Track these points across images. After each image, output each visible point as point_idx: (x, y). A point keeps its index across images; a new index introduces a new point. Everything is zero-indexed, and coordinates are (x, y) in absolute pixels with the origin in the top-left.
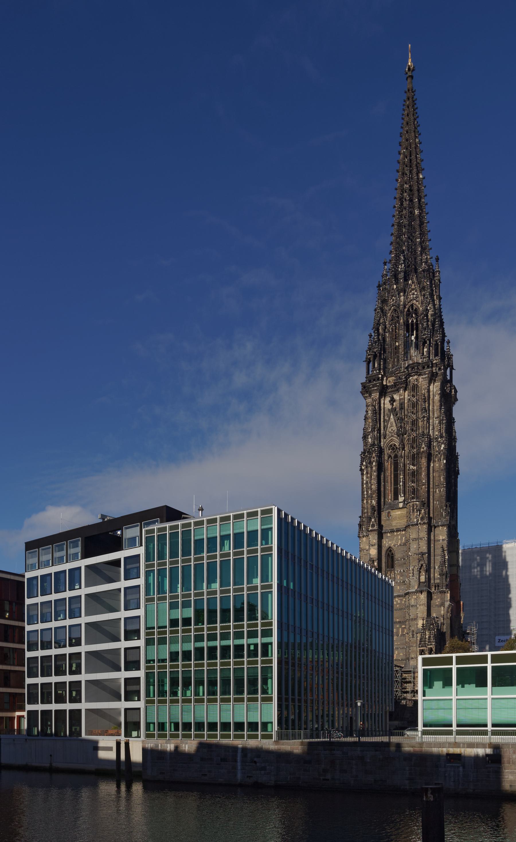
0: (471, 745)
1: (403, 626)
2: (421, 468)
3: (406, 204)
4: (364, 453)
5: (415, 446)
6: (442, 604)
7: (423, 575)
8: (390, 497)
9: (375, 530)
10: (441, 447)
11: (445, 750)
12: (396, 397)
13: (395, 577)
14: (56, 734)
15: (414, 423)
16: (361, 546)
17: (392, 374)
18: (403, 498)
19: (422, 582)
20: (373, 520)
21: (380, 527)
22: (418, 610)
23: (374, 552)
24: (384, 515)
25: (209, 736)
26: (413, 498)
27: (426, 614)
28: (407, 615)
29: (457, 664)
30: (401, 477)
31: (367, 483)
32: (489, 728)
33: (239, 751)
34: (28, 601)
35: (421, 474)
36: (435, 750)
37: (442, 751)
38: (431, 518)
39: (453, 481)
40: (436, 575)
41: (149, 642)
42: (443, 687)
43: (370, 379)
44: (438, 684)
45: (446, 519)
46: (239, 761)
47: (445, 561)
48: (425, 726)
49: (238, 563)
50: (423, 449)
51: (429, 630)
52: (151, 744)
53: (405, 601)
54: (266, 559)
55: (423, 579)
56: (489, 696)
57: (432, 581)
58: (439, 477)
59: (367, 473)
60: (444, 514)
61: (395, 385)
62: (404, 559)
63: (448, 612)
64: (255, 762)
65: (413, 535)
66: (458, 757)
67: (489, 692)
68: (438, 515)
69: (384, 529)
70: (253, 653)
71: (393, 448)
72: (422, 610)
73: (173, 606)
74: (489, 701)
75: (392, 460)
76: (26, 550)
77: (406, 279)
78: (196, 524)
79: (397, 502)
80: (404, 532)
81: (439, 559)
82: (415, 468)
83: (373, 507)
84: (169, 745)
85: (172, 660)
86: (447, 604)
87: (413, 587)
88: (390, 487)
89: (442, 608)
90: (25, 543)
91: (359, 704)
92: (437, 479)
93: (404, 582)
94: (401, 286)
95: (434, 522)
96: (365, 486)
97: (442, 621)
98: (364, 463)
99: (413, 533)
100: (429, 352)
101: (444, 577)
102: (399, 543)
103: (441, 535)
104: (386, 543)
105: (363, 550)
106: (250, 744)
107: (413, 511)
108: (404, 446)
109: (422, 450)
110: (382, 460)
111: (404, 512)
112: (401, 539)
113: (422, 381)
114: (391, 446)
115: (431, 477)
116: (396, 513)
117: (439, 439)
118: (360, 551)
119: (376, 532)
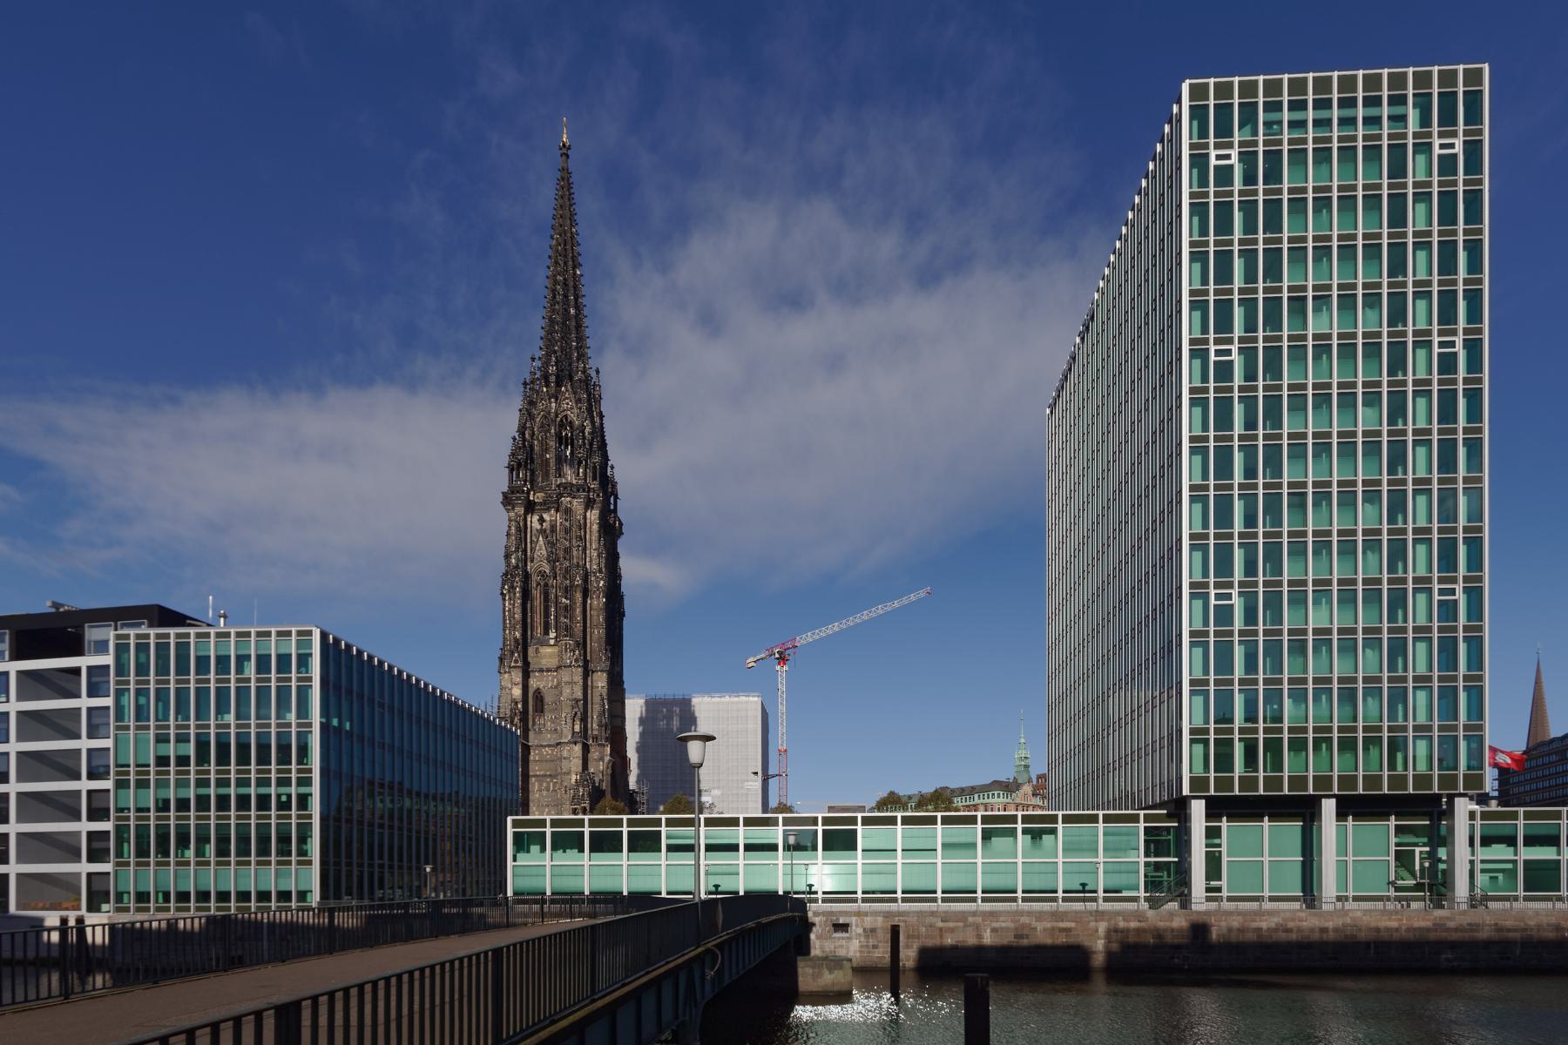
3: (559, 298)
4: (506, 574)
6: (602, 759)
8: (539, 631)
12: (546, 516)
15: (568, 551)
17: (542, 490)
21: (526, 664)
23: (517, 692)
24: (531, 651)
25: (218, 909)
32: (899, 895)
41: (121, 784)
43: (513, 490)
44: (535, 849)
45: (605, 665)
49: (263, 693)
54: (303, 693)
55: (577, 728)
56: (625, 862)
58: (597, 617)
61: (544, 503)
65: (566, 679)
70: (284, 806)
71: (542, 574)
72: (576, 764)
73: (162, 739)
74: (899, 867)
77: (559, 384)
78: (218, 635)
81: (597, 708)
83: (516, 640)
85: (158, 809)
86: (607, 758)
88: (538, 619)
94: (553, 391)
95: (591, 666)
99: (565, 675)
100: (585, 473)
103: (600, 681)
104: (534, 683)
105: (485, 690)
111: (556, 650)
113: (577, 505)
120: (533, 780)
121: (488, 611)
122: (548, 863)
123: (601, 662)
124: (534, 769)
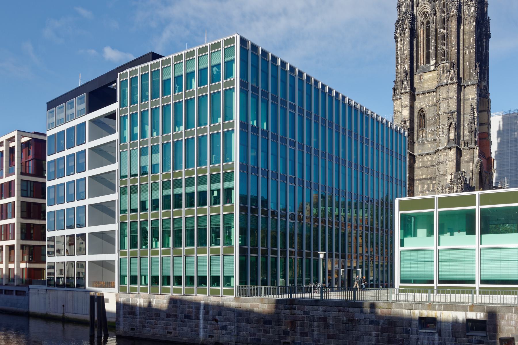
0: (449, 307)
1: (434, 182)
2: (451, 31)
4: (398, 21)
5: (445, 10)
6: (472, 160)
7: (452, 133)
8: (422, 60)
9: (407, 92)
10: (471, 10)
11: (417, 313)
13: (426, 136)
14: (78, 286)
16: (395, 109)
18: (435, 61)
19: (452, 139)
20: (405, 83)
21: (413, 89)
22: (448, 165)
23: (406, 113)
24: (416, 78)
26: (443, 60)
27: (454, 169)
28: (437, 171)
29: (439, 207)
30: (433, 41)
31: (401, 49)
33: (202, 308)
34: (49, 158)
35: (451, 37)
36: (406, 312)
37: (414, 313)
38: (461, 78)
39: (484, 44)
40: (466, 133)
42: (427, 236)
44: (422, 232)
45: (475, 79)
46: (201, 318)
47: (474, 118)
48: (402, 281)
50: (453, 12)
51: (457, 184)
52: (123, 298)
53: (436, 158)
55: (452, 136)
57: (462, 139)
58: (469, 39)
59: (401, 40)
60: (474, 74)
62: (435, 119)
63: (477, 167)
64: (217, 321)
65: (443, 95)
66: (434, 320)
67: (474, 241)
68: (467, 75)
69: (416, 91)
71: (426, 15)
72: (451, 166)
75: (425, 26)
76: (48, 110)
79: (428, 65)
80: (435, 93)
81: (468, 117)
82: (445, 31)
83: (405, 71)
84: (138, 299)
86: (476, 159)
87: (443, 144)
88: (422, 52)
89: (471, 164)
90: (48, 103)
91: (322, 256)
92: (467, 41)
93: (435, 140)
95: (463, 83)
96: (399, 52)
97: (471, 176)
98: (398, 31)
99: (443, 93)
101: (473, 134)
102: (431, 103)
103: (471, 94)
104: (418, 104)
105: (394, 112)
106: (212, 300)
107: (443, 72)
108: (436, 12)
109: (452, 13)
110: (414, 27)
112: (433, 100)
114: (424, 13)
115: (461, 39)
116: (428, 76)
117: (469, 3)
118: (395, 113)
119: (409, 94)
120: (417, 183)
121: (387, 48)
122: (434, 246)
123: (471, 76)
124: (418, 174)
